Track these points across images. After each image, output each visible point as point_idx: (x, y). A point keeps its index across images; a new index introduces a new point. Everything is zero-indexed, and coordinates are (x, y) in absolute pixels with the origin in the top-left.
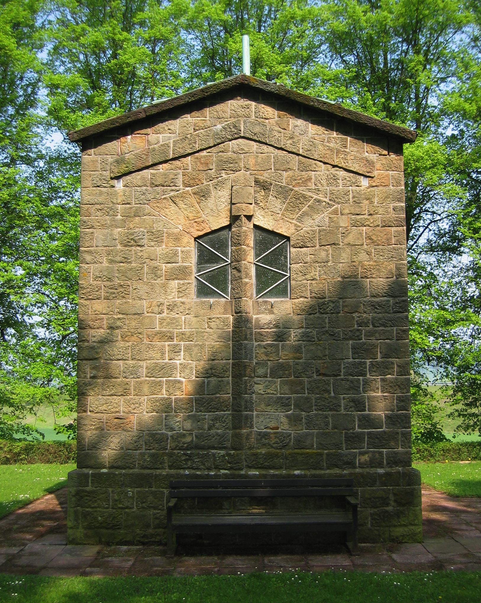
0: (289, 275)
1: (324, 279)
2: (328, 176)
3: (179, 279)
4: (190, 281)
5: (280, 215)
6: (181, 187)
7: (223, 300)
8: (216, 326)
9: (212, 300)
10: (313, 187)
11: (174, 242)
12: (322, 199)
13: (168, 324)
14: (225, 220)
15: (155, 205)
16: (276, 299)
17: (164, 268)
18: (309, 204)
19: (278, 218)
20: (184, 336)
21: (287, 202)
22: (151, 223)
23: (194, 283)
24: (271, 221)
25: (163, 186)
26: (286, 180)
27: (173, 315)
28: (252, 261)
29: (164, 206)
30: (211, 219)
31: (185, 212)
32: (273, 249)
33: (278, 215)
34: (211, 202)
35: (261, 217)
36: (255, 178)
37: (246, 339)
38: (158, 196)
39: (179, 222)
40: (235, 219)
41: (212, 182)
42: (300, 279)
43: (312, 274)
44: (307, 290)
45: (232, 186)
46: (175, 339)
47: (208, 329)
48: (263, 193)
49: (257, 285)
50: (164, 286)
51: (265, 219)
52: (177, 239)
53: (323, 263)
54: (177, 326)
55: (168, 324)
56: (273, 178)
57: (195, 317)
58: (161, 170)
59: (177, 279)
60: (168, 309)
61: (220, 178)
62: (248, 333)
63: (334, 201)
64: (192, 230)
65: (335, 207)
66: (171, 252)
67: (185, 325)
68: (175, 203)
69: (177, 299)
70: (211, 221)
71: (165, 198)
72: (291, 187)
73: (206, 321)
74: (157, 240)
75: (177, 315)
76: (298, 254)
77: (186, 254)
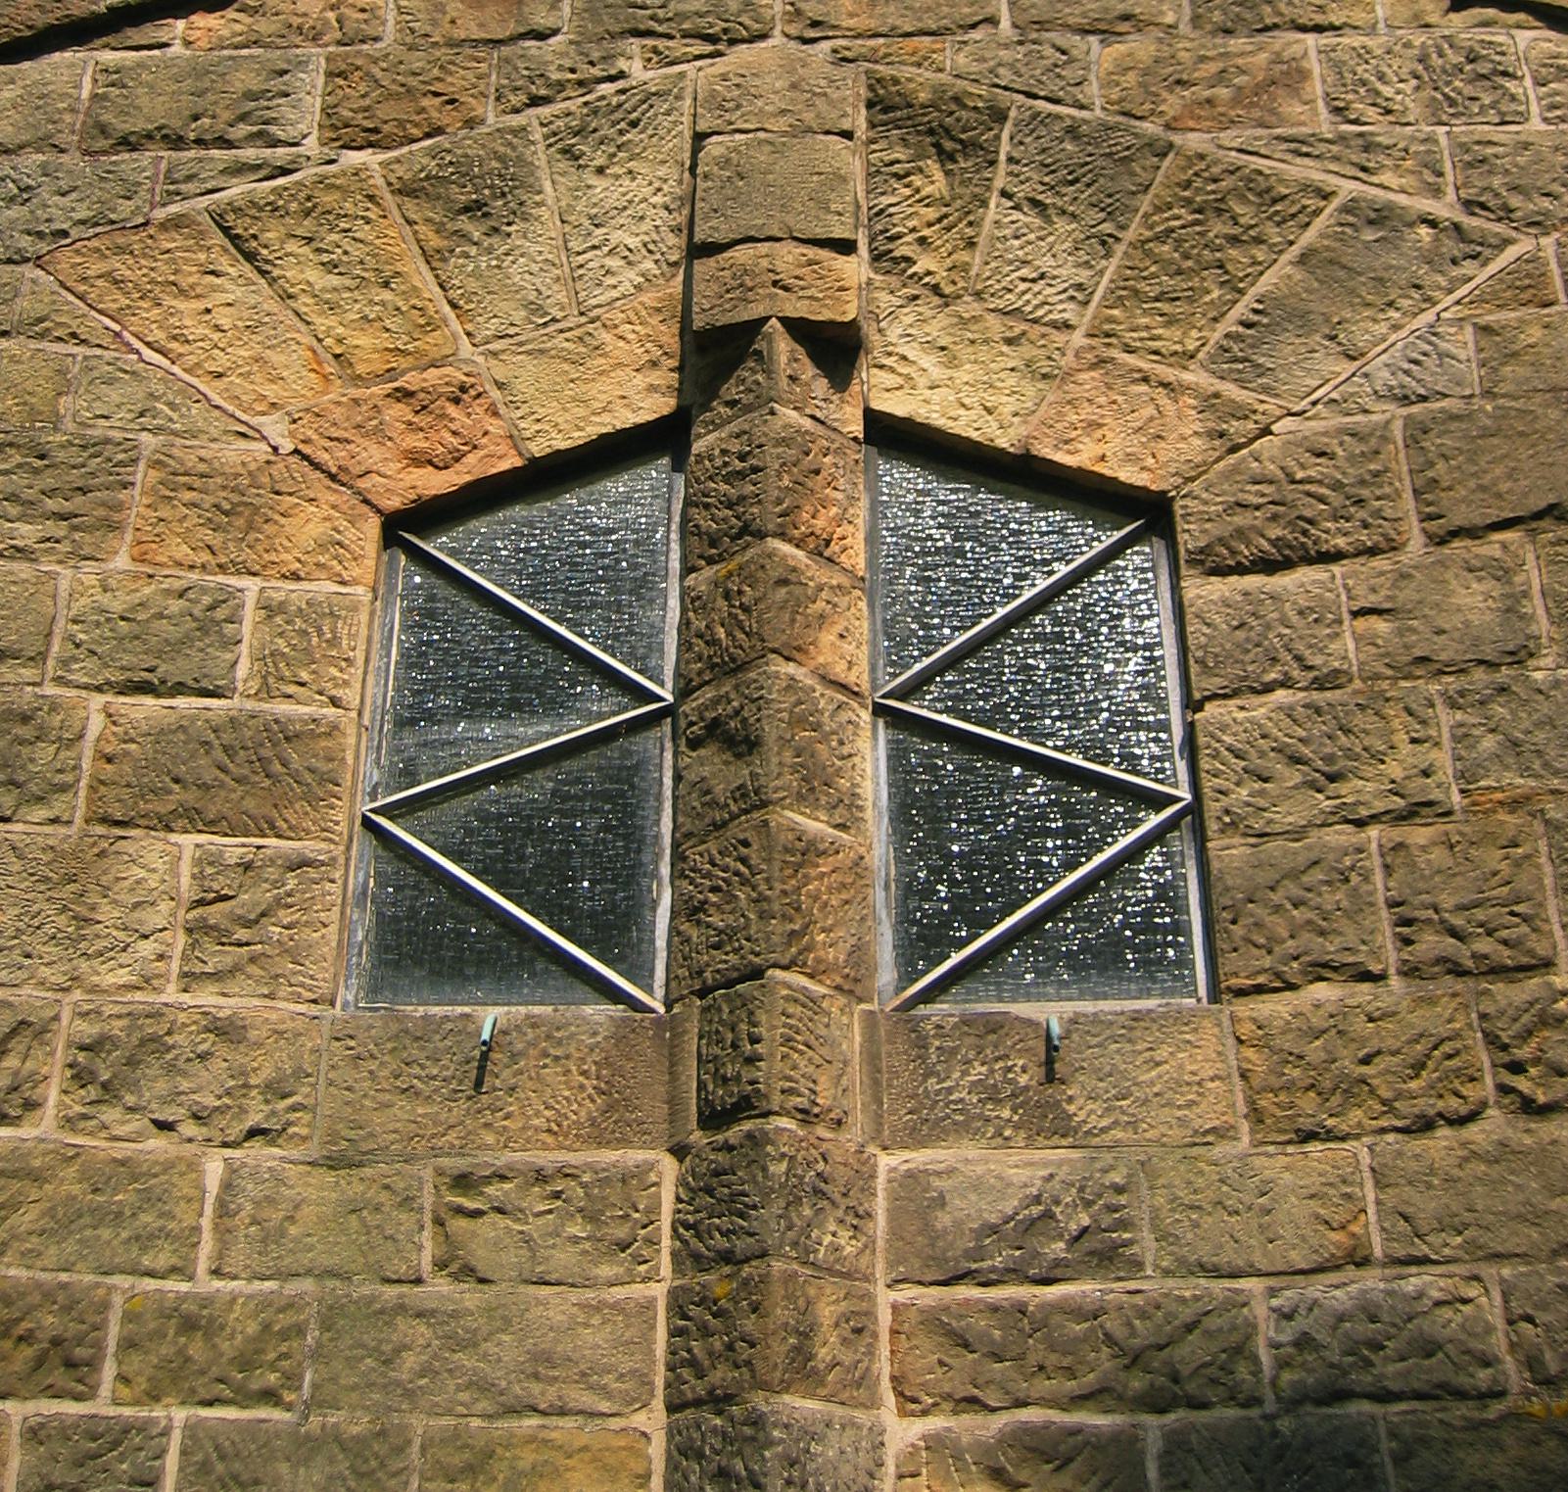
0: (1185, 794)
1: (1515, 804)
2: (1422, 59)
3: (211, 826)
4: (310, 847)
5: (1078, 339)
6: (311, 146)
7: (599, 1012)
8: (514, 1257)
9: (490, 1018)
10: (1325, 124)
11: (208, 536)
12: (1402, 200)
13: (62, 1221)
14: (640, 381)
15: (96, 268)
16: (1088, 1007)
17: (96, 724)
18: (1309, 237)
19: (1068, 361)
20: (197, 1349)
21: (1129, 235)
22: (46, 389)
23: (358, 869)
24: (1011, 380)
25: (177, 142)
26: (1107, 84)
27: (123, 1136)
28: (859, 676)
29: (164, 271)
30: (525, 374)
31: (321, 323)
32: (1009, 922)
33: (1059, 338)
34: (531, 257)
35: (928, 361)
36: (875, 82)
37: (803, 1371)
38: (125, 208)
39: (271, 391)
40: (715, 354)
41: (545, 111)
42: (1287, 816)
43: (1393, 769)
44: (1360, 905)
45: (699, 138)
46: (109, 1370)
47: (440, 1287)
48: (936, 182)
49: (911, 892)
50: (73, 878)
51: (962, 375)
52: (240, 511)
53: (1479, 675)
54: (144, 1240)
55: (62, 1221)
56: (1006, 76)
57: (333, 1163)
58: (177, 49)
59: (194, 819)
60: (81, 1077)
61: (606, 88)
62: (827, 1312)
63: (1506, 214)
64: (371, 454)
65: (1511, 253)
66: (175, 606)
67: (223, 1232)
68: (250, 257)
69: (171, 994)
70: (523, 387)
71: (175, 223)
72: (1149, 128)
73: (427, 1200)
74: (68, 506)
75: (158, 1144)
76: (1245, 617)
77: (301, 642)
